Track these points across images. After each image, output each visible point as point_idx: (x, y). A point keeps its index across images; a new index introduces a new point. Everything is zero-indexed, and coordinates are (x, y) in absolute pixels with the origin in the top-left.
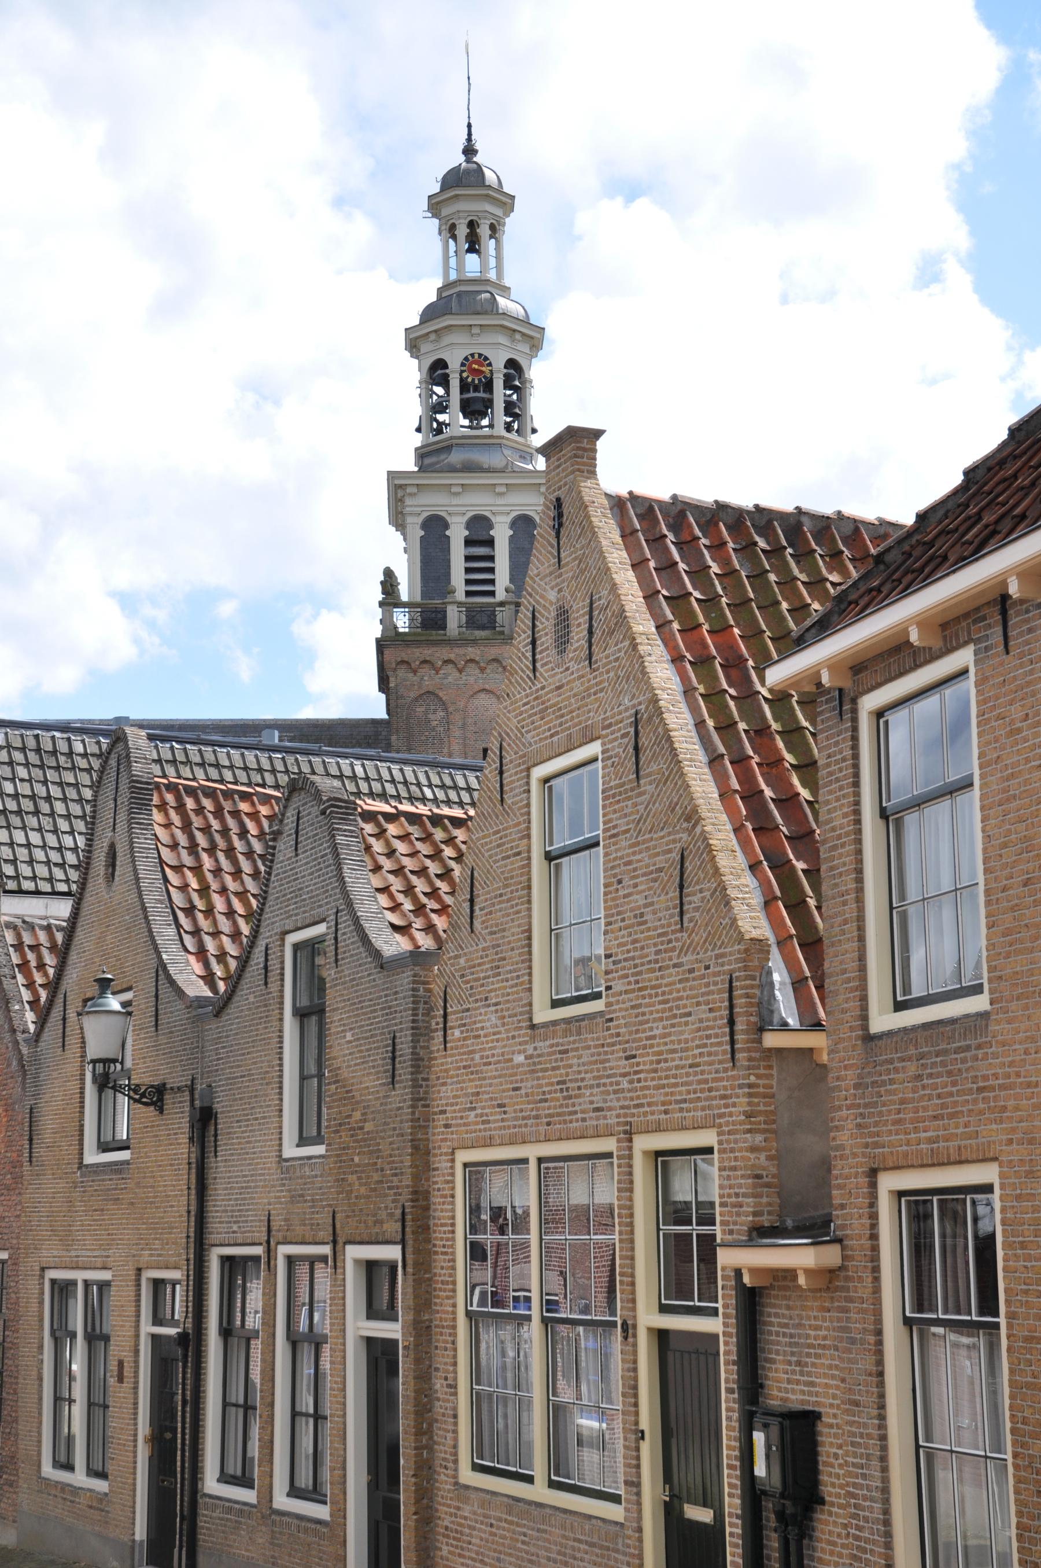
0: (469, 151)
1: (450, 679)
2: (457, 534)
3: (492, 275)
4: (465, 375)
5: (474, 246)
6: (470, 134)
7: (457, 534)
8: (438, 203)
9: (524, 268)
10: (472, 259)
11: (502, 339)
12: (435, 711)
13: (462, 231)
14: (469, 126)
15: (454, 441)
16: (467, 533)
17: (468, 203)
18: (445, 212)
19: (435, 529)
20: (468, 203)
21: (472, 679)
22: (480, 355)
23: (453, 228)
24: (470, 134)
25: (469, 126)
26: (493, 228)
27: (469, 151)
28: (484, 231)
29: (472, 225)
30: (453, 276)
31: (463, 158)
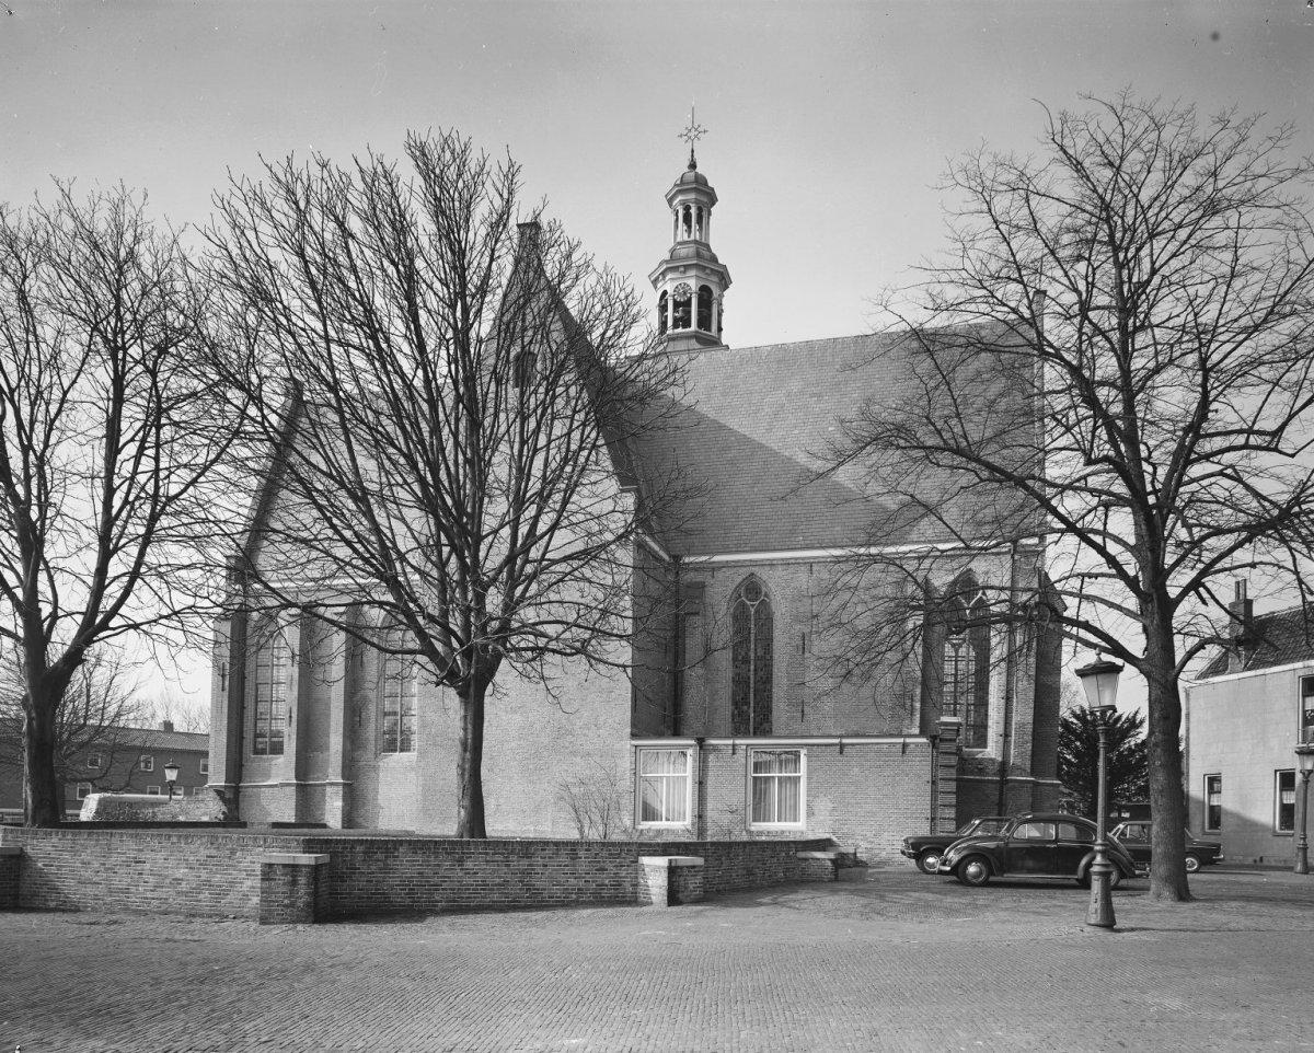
0: (693, 166)
17: (696, 199)
27: (693, 166)
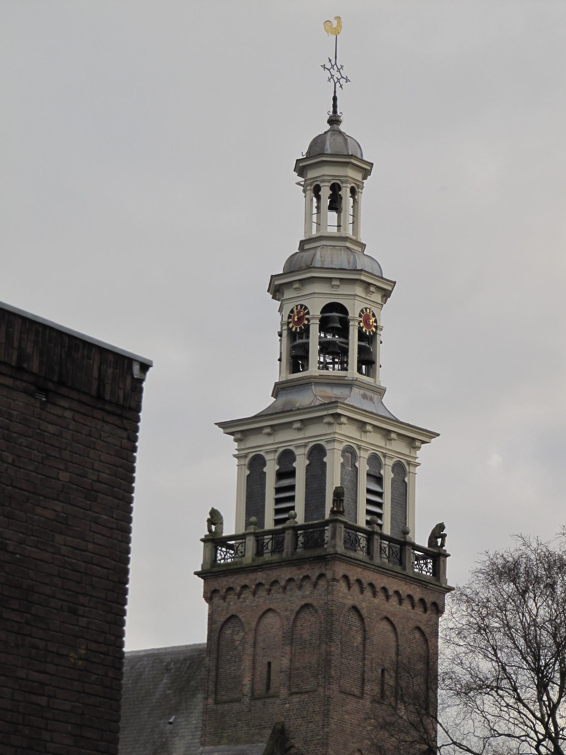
0: (334, 121)
1: (248, 602)
2: (271, 469)
3: (350, 233)
4: (291, 325)
5: (335, 204)
6: (335, 106)
7: (271, 469)
8: (304, 167)
9: (382, 223)
10: (332, 216)
11: (359, 290)
12: (238, 631)
13: (326, 192)
14: (335, 99)
15: (357, 383)
16: (277, 467)
17: (331, 169)
18: (311, 174)
19: (256, 464)
20: (331, 169)
21: (261, 600)
22: (302, 306)
23: (317, 190)
24: (335, 106)
25: (335, 99)
26: (353, 192)
27: (334, 121)
28: (345, 193)
29: (336, 188)
30: (314, 233)
31: (328, 127)
